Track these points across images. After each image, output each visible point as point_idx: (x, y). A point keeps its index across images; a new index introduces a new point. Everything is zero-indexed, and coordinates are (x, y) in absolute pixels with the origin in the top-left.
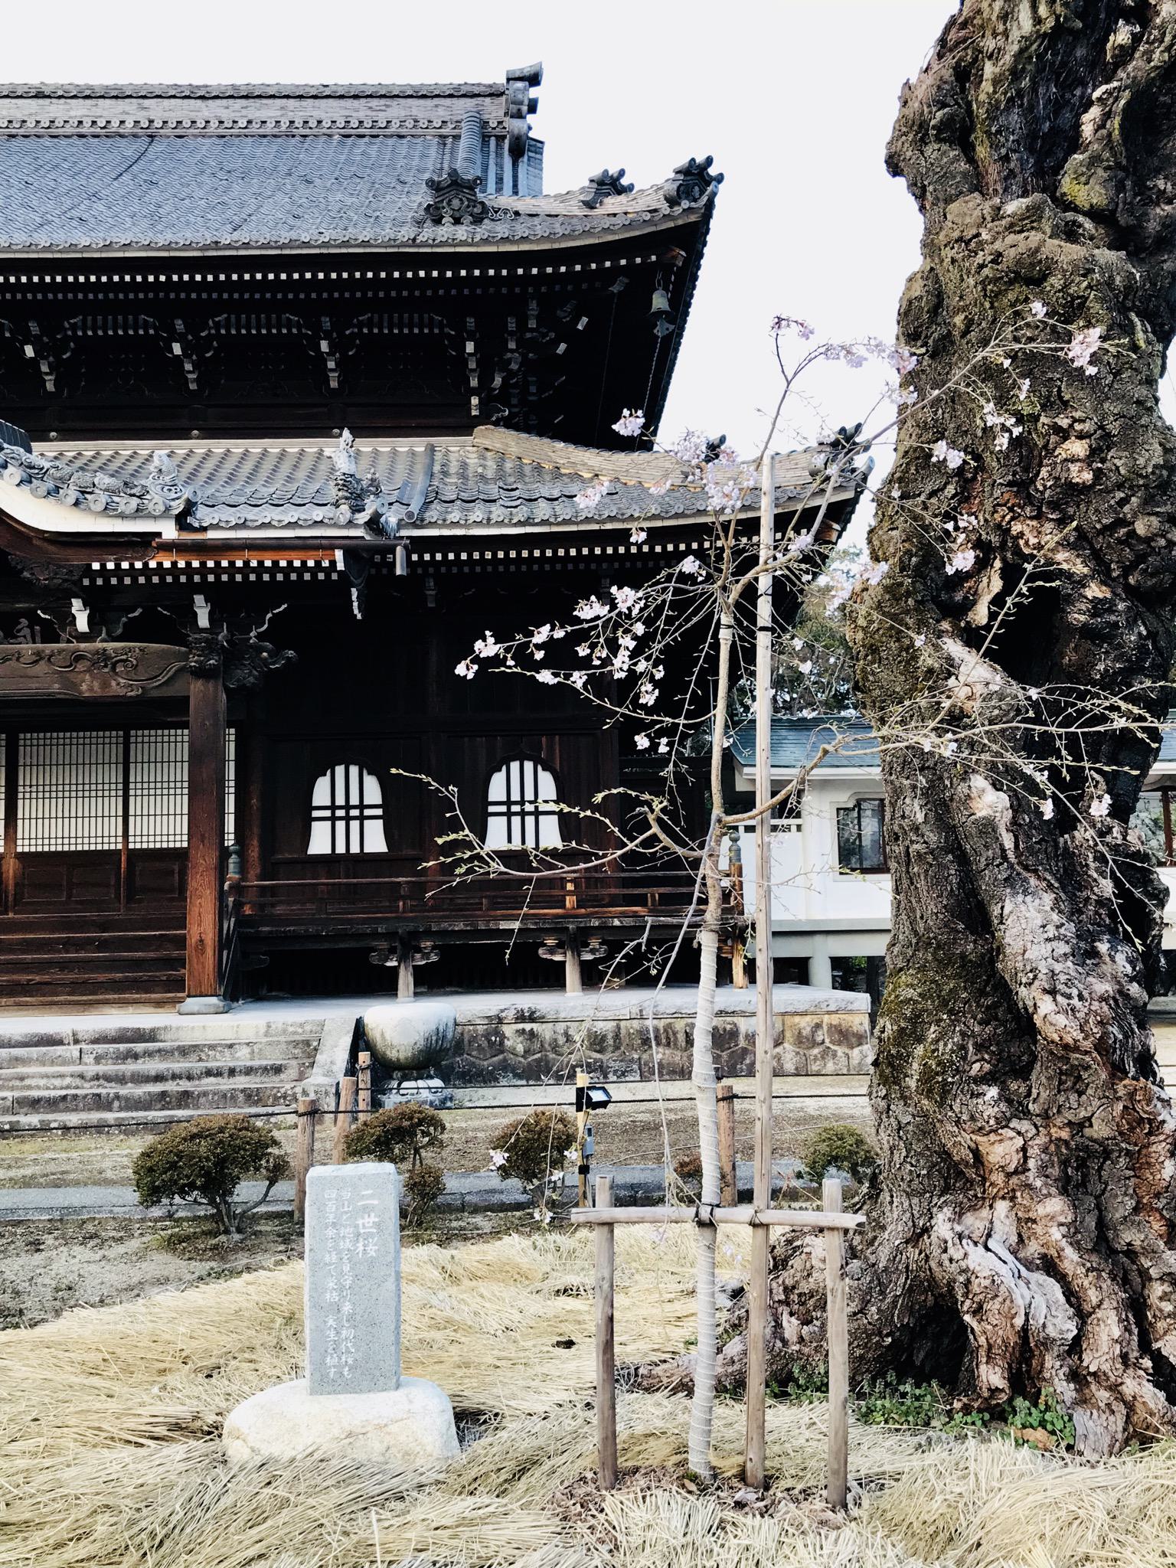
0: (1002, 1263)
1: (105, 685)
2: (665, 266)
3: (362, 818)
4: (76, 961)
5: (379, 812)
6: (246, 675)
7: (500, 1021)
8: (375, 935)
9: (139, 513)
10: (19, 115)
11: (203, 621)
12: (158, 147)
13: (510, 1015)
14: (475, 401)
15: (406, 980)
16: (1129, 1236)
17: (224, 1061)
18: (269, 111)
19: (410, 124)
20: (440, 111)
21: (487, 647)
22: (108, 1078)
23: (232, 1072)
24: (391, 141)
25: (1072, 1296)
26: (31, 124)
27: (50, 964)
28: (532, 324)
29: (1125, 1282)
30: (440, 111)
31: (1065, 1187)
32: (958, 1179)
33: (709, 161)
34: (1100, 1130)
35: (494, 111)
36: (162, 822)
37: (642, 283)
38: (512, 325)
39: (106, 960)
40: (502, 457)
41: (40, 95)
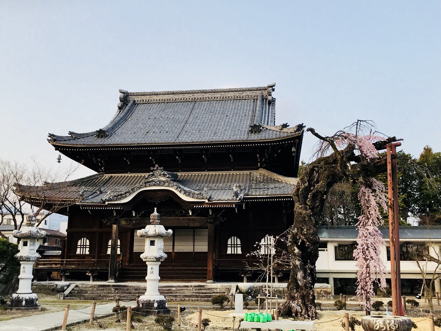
0: (295, 305)
1: (194, 224)
2: (295, 143)
3: (237, 247)
4: (187, 273)
5: (240, 246)
6: (218, 223)
7: (262, 287)
8: (239, 270)
9: (202, 198)
10: (169, 98)
11: (211, 213)
12: (197, 105)
13: (264, 286)
14: (259, 164)
15: (245, 279)
16: (307, 303)
17: (215, 291)
18: (218, 95)
19: (247, 97)
20: (254, 94)
21: (248, 255)
22: (197, 293)
23: (217, 293)
24: (243, 101)
25: (301, 308)
26: (172, 100)
27: (183, 273)
28: (270, 150)
29: (306, 307)
30: (254, 94)
31: (302, 299)
32: (293, 298)
33: (303, 124)
34: (305, 294)
35: (265, 93)
36: (202, 247)
37: (291, 145)
38: (266, 150)
39: (192, 273)
40: (264, 176)
41: (174, 94)
